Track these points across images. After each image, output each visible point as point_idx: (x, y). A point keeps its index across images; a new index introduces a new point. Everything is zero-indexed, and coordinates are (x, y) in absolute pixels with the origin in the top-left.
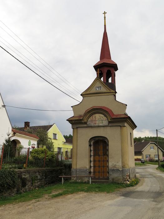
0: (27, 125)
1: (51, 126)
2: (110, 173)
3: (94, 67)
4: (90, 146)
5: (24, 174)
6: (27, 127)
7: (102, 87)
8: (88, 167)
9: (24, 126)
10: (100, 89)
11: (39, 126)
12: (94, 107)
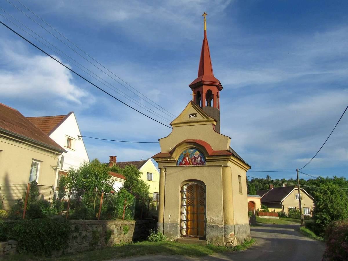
0: (113, 160)
1: (144, 162)
2: (208, 230)
3: (190, 86)
4: (182, 192)
5: (96, 225)
6: (112, 163)
7: (198, 114)
8: (179, 221)
9: (109, 162)
10: (195, 117)
11: (128, 162)
12: (187, 140)
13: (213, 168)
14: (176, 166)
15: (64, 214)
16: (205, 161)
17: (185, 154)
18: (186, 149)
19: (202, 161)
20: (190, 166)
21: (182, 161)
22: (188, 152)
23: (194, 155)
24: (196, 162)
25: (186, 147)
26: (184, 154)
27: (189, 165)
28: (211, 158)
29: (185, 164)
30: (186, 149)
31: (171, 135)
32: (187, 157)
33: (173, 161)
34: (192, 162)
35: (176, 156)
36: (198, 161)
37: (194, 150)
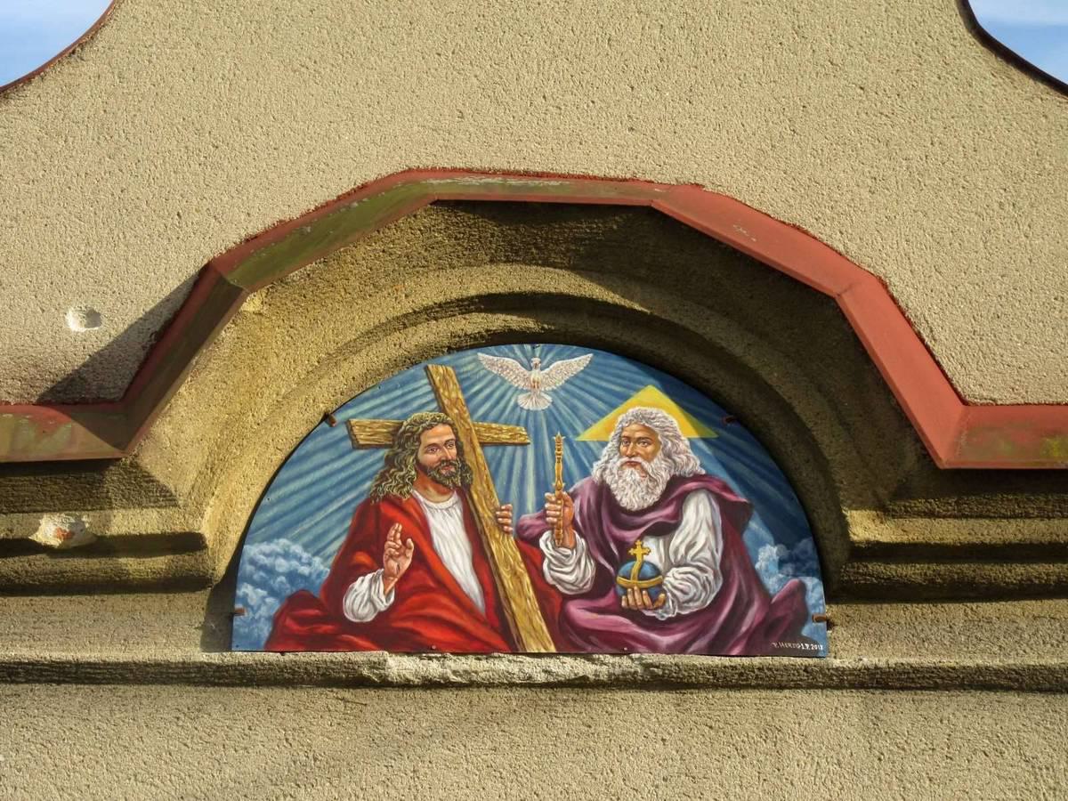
13: (961, 711)
14: (202, 657)
15: (262, 577)
16: (815, 589)
17: (403, 439)
18: (425, 334)
19: (754, 578)
20: (503, 665)
21: (344, 574)
22: (453, 393)
23: (585, 457)
24: (635, 599)
25: (390, 306)
26: (368, 422)
27: (484, 651)
28: (948, 531)
29: (386, 633)
30: (425, 334)
31: (91, 64)
32: (443, 487)
33: (132, 565)
34: (547, 595)
35: (212, 470)
36: (673, 578)
37: (581, 361)
